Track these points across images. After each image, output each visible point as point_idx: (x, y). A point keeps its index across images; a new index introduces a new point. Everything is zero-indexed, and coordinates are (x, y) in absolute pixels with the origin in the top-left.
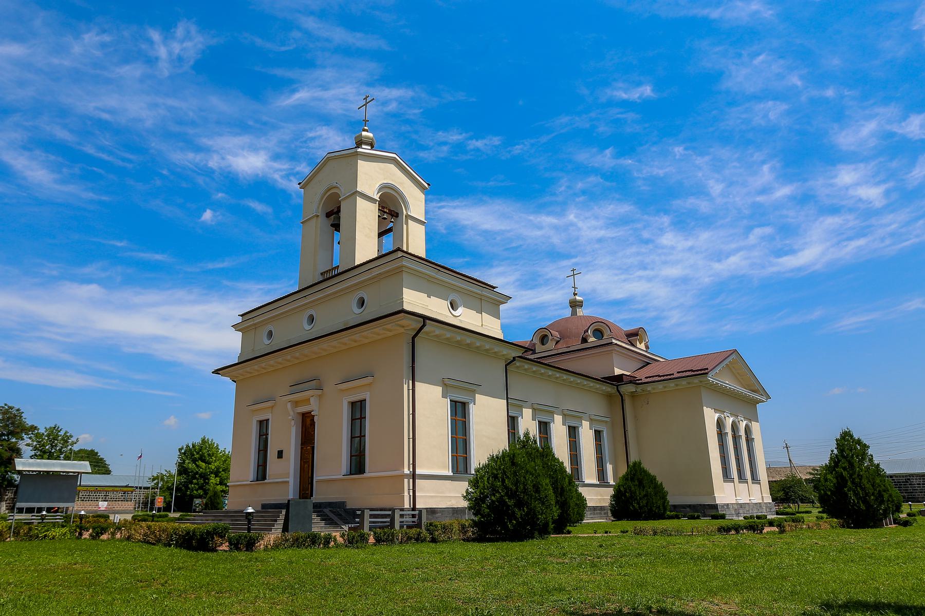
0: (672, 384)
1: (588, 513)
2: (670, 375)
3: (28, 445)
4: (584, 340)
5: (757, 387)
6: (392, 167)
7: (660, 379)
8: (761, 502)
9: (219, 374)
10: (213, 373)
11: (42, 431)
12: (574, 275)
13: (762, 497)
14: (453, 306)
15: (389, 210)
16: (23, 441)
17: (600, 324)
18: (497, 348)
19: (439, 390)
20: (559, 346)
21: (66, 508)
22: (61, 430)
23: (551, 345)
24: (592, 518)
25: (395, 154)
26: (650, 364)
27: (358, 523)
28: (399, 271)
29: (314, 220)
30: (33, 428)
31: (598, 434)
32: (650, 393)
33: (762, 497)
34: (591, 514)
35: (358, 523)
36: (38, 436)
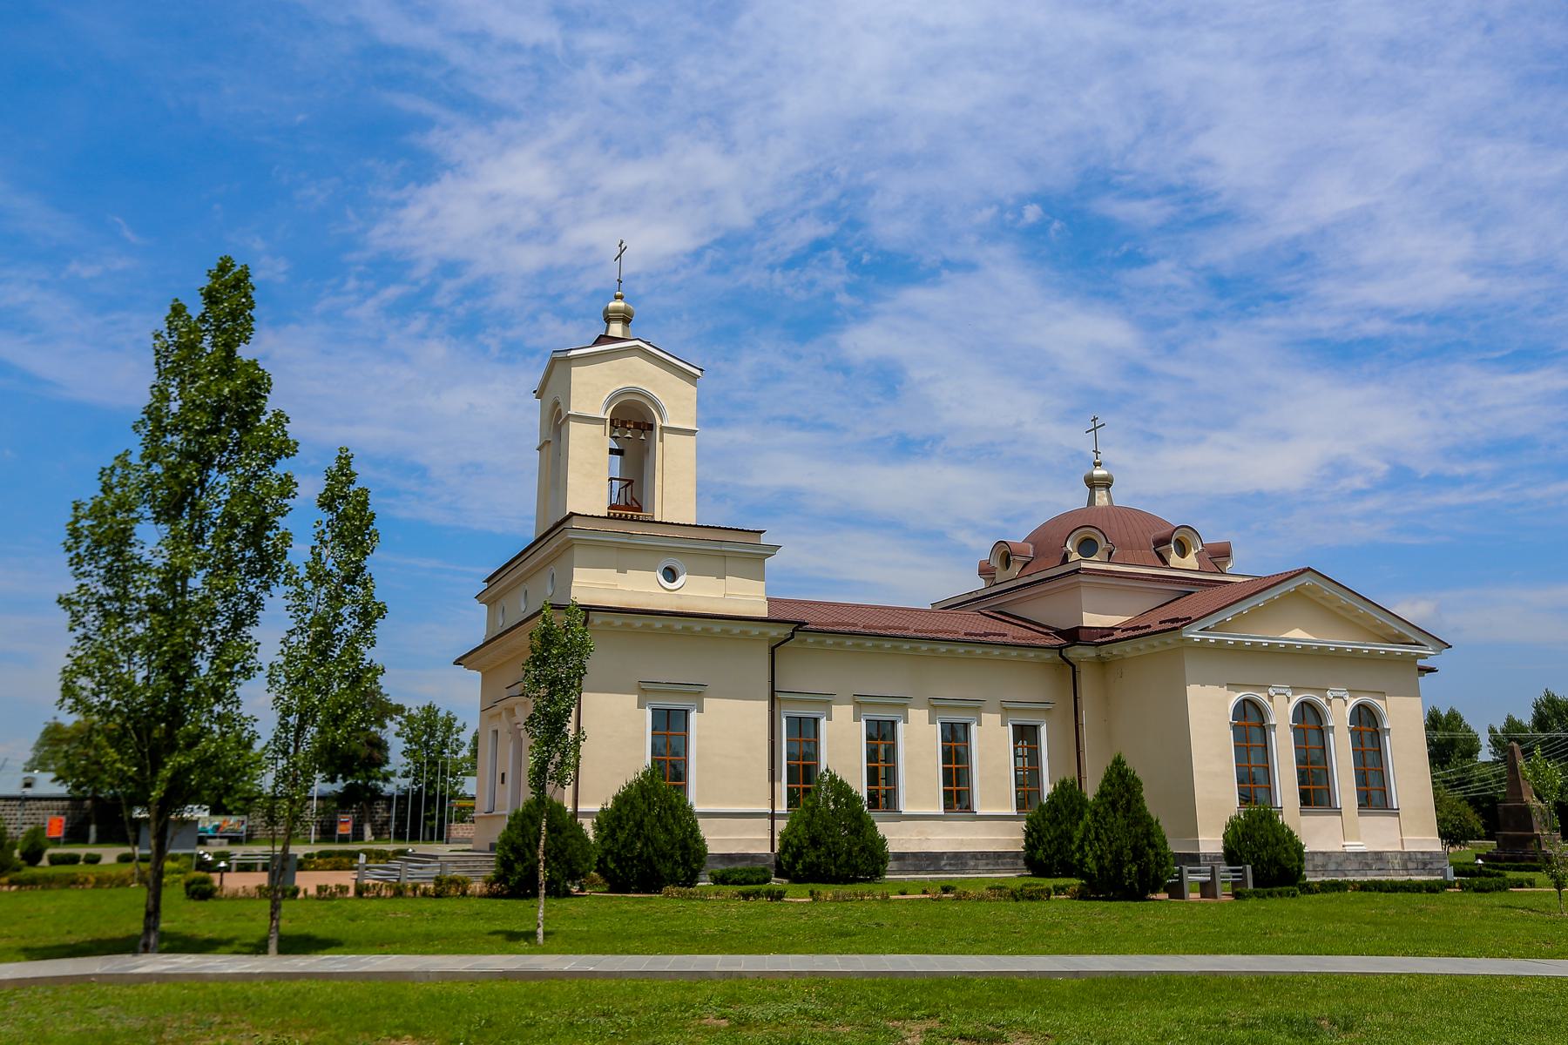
0: (1155, 641)
1: (891, 865)
2: (1145, 627)
3: (398, 735)
4: (1065, 560)
5: (1398, 628)
6: (636, 361)
7: (1136, 633)
8: (1401, 850)
9: (461, 664)
10: (455, 663)
11: (414, 712)
12: (1095, 429)
13: (1402, 840)
14: (671, 574)
15: (635, 424)
16: (386, 730)
17: (1088, 529)
18: (755, 630)
19: (633, 699)
20: (1028, 571)
21: (1398, 813)
22: (438, 710)
23: (1015, 569)
24: (988, 871)
25: (638, 339)
26: (1193, 592)
27: (1176, 878)
28: (569, 545)
29: (546, 446)
30: (399, 709)
31: (1025, 735)
32: (1124, 658)
33: (1402, 840)
34: (987, 864)
35: (1176, 878)
36: (410, 719)
